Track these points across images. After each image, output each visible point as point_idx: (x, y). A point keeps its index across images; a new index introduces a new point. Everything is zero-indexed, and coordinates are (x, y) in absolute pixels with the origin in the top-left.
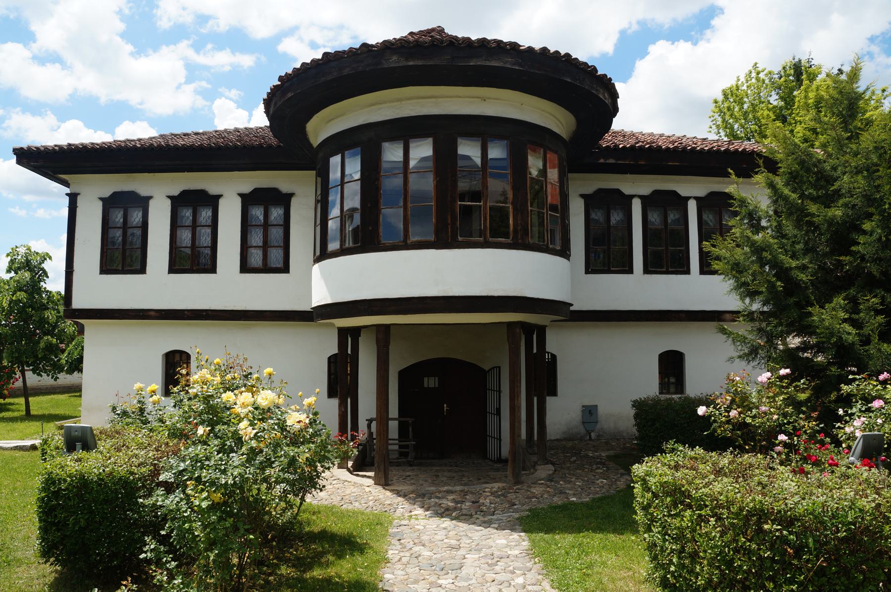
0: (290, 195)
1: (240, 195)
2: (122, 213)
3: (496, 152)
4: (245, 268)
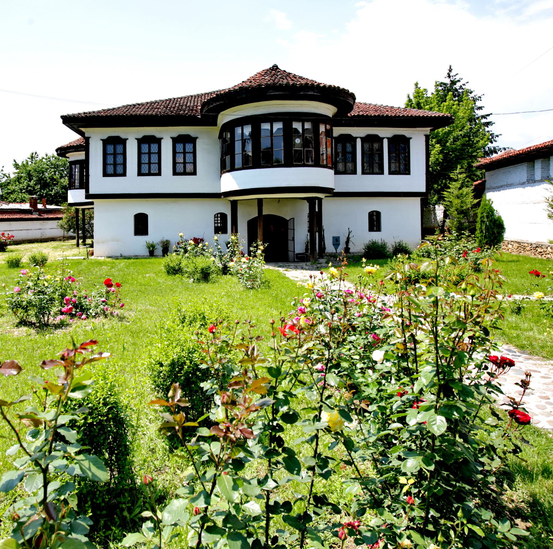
0: (126, 140)
1: (172, 138)
2: (113, 146)
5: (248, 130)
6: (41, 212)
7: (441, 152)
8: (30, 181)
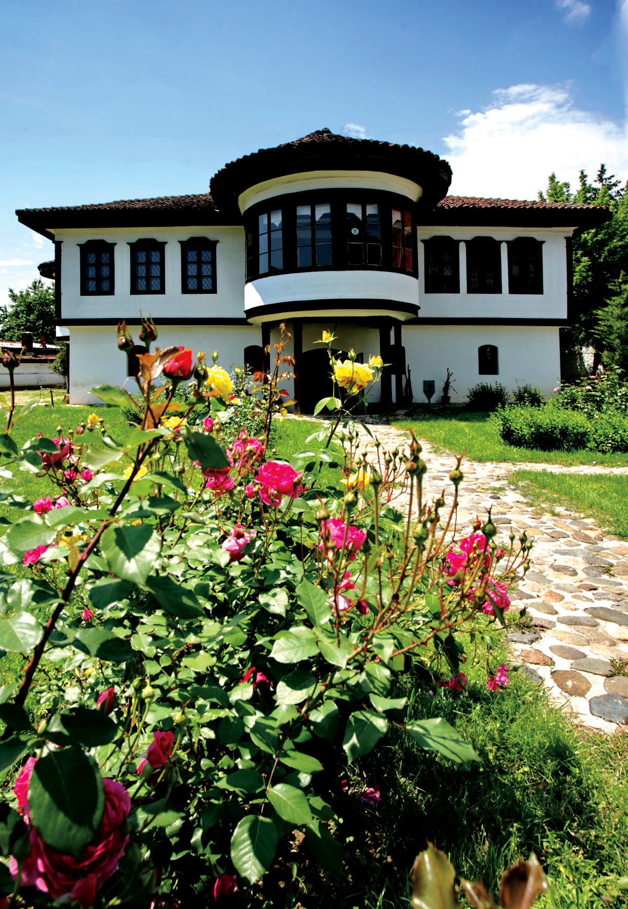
3: (371, 210)
4: (185, 290)
5: (277, 219)
6: (37, 351)
7: (589, 268)
8: (28, 315)
